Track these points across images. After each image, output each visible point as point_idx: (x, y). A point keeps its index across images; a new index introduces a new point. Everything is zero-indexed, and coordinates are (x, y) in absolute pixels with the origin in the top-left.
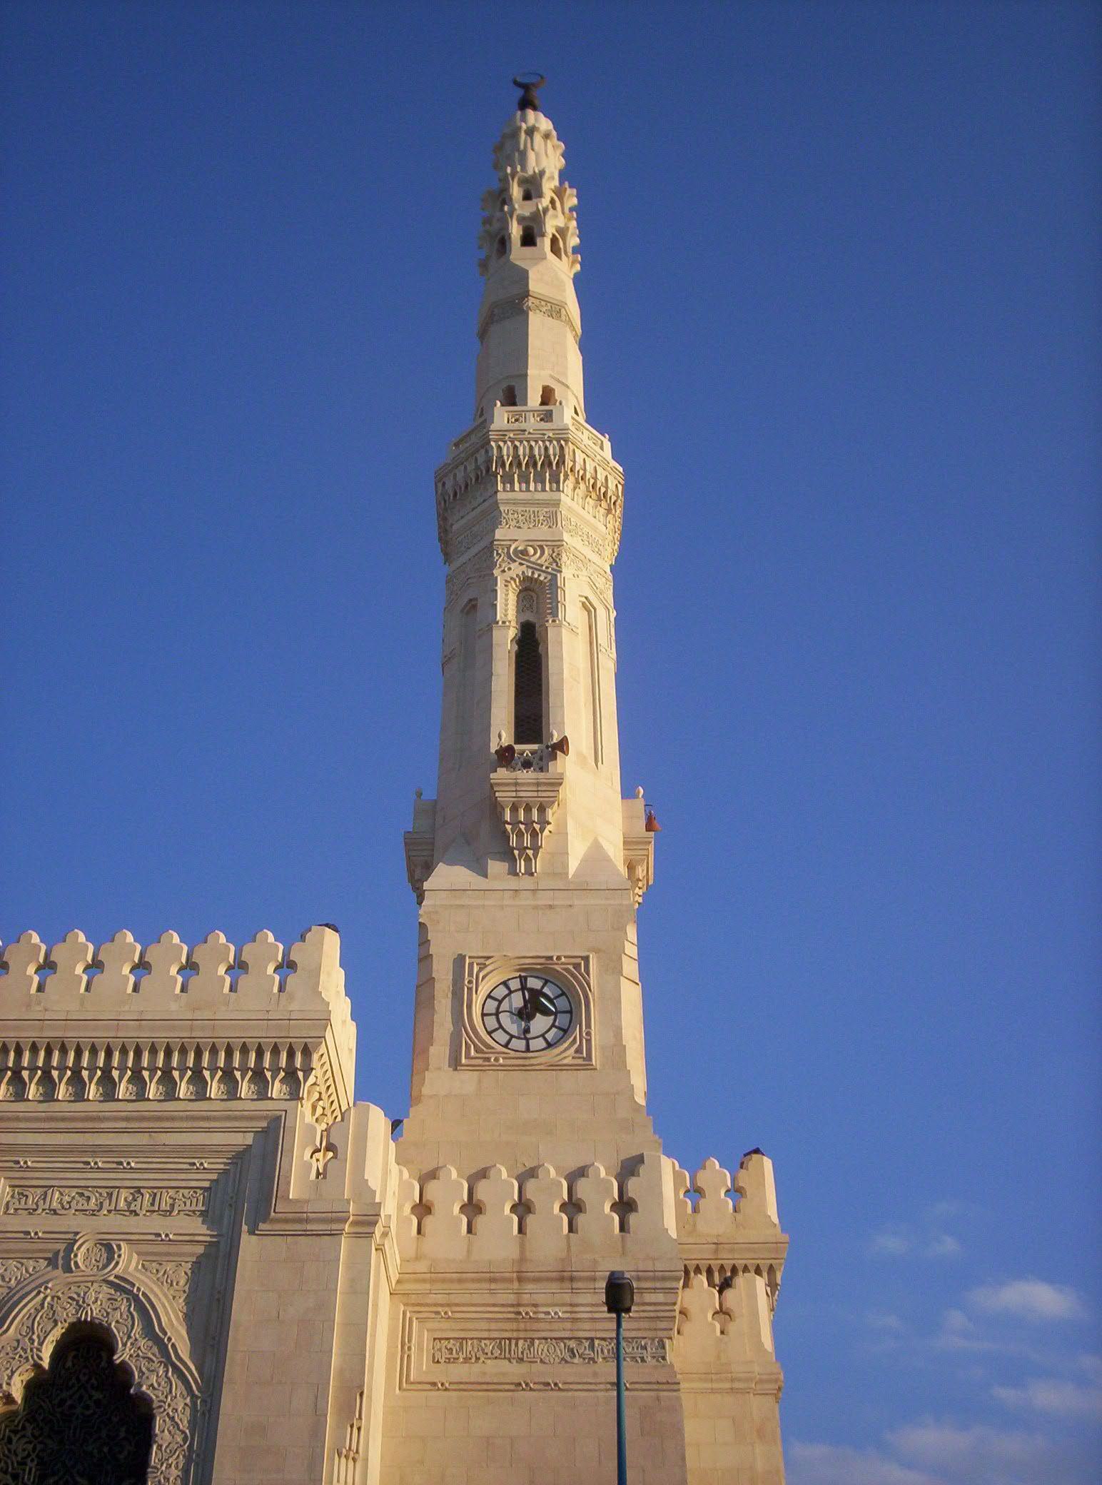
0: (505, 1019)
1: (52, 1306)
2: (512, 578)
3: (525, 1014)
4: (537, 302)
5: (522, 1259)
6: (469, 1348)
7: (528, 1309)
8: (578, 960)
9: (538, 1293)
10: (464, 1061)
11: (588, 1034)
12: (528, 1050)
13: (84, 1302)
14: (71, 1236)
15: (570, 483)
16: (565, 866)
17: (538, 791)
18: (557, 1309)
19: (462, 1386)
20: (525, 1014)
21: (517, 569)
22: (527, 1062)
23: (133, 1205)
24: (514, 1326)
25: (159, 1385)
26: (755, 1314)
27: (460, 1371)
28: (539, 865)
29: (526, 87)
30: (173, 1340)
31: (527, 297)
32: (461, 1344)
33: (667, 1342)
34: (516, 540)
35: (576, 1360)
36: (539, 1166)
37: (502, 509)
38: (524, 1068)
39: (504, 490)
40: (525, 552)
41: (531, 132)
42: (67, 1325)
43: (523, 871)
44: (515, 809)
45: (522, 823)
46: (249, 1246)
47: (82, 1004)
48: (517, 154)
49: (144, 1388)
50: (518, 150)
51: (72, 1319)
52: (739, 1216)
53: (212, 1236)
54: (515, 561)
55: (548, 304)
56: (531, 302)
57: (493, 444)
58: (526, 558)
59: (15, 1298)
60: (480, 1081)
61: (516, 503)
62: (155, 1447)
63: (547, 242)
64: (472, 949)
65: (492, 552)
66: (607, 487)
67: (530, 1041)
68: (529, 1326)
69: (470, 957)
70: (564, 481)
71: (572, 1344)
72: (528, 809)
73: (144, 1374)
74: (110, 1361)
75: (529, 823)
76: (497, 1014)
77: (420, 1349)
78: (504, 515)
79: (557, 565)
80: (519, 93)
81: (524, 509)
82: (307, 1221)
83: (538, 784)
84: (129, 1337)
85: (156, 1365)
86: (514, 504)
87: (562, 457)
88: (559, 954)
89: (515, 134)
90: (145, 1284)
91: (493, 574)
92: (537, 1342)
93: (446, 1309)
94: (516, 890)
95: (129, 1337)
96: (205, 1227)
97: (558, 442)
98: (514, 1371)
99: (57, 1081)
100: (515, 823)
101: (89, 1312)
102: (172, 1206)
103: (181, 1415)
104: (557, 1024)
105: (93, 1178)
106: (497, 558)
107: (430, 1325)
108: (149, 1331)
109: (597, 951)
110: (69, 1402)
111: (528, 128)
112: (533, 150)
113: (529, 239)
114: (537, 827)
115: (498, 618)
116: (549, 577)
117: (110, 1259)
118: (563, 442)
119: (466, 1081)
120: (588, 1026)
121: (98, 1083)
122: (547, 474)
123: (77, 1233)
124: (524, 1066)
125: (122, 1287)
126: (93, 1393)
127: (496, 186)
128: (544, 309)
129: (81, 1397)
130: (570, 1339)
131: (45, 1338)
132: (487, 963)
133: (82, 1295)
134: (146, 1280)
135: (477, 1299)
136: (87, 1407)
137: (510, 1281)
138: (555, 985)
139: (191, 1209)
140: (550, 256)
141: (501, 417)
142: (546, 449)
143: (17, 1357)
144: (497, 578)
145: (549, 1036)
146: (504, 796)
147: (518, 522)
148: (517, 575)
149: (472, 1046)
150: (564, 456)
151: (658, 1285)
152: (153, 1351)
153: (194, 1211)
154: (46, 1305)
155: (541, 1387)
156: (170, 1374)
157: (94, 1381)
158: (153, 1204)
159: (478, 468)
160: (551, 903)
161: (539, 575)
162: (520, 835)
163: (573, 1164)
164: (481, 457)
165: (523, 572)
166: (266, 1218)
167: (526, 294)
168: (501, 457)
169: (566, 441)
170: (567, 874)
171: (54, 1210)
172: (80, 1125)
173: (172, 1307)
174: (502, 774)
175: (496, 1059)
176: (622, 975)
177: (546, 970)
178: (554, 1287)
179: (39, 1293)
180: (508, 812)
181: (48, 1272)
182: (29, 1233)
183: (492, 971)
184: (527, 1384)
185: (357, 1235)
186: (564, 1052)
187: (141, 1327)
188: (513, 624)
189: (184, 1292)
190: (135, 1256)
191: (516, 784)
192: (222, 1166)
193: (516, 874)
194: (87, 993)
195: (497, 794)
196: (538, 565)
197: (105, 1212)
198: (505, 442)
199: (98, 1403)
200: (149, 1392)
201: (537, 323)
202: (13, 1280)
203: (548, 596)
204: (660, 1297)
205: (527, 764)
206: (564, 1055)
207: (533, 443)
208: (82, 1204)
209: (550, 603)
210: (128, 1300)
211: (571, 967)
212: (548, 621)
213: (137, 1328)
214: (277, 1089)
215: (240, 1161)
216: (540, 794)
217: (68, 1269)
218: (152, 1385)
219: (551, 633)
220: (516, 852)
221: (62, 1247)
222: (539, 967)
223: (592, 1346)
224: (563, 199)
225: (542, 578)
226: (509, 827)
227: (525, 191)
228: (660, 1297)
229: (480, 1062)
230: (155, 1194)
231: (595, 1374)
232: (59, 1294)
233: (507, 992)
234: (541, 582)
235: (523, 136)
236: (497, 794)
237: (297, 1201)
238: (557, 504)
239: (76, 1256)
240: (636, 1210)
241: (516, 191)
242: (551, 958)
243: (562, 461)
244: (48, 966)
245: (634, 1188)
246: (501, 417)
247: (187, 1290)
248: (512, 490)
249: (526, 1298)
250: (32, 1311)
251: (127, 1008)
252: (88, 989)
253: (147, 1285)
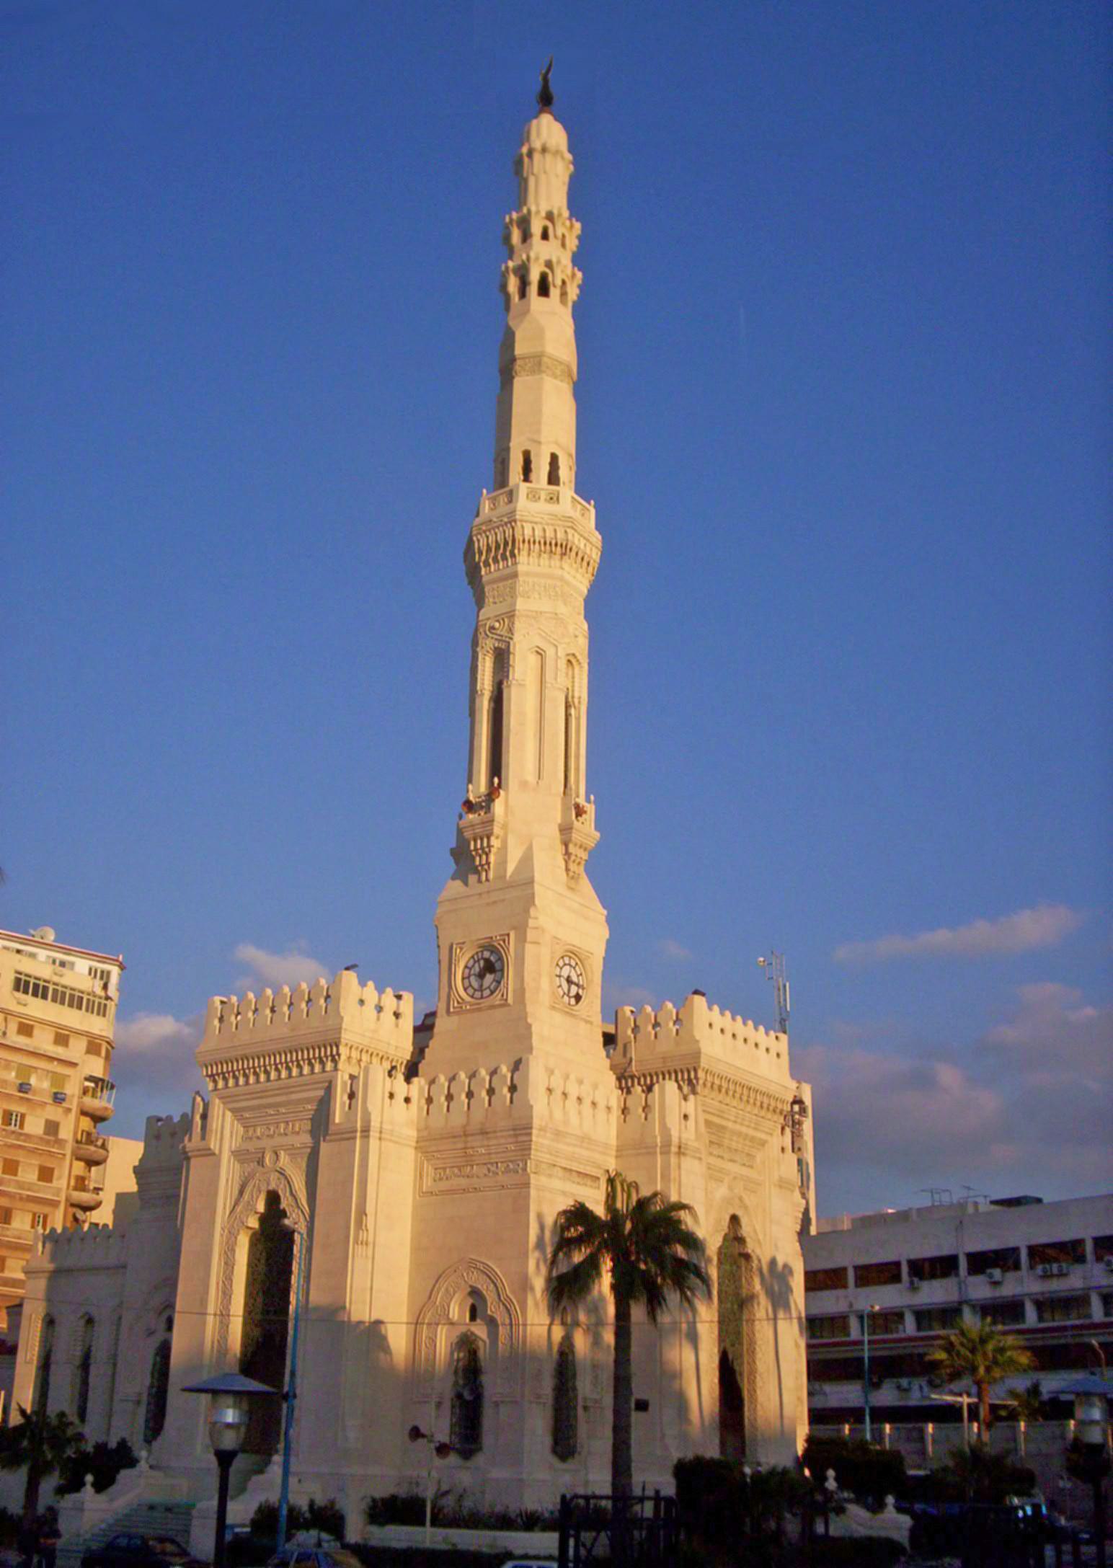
0: (472, 978)
3: (481, 976)
15: (524, 553)
16: (505, 871)
20: (481, 976)
24: (464, 1159)
35: (491, 1174)
52: (678, 1038)
74: (279, 1208)
98: (463, 1182)
107: (432, 1162)
109: (514, 928)
114: (487, 850)
137: (460, 1136)
170: (505, 876)
172: (259, 1095)
178: (480, 1137)
190: (229, 1114)
214: (329, 1066)
217: (263, 1166)
220: (480, 868)
237: (337, 1124)
249: (469, 1145)
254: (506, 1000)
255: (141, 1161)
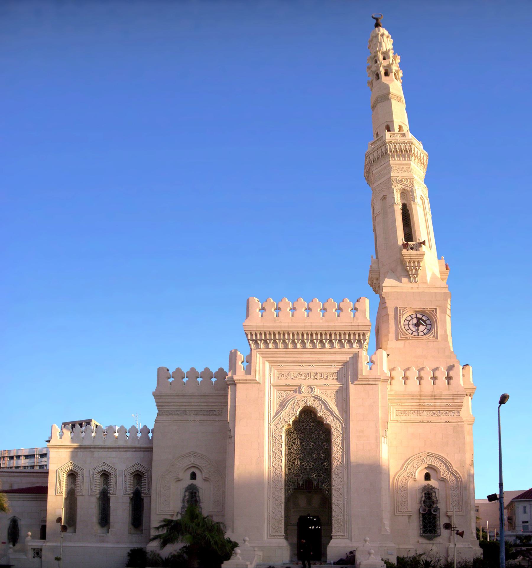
0: (411, 326)
1: (298, 403)
2: (398, 189)
3: (417, 325)
4: (393, 96)
5: (421, 391)
6: (406, 413)
7: (422, 403)
8: (433, 309)
9: (426, 400)
10: (399, 338)
11: (437, 331)
12: (418, 335)
13: (307, 401)
14: (299, 385)
16: (426, 280)
17: (417, 257)
18: (430, 403)
19: (405, 421)
20: (417, 325)
21: (400, 186)
22: (419, 339)
23: (315, 377)
24: (419, 407)
25: (332, 421)
26: (468, 406)
27: (404, 418)
28: (418, 279)
29: (377, 19)
30: (334, 411)
31: (390, 94)
32: (404, 411)
33: (460, 412)
34: (398, 177)
36: (425, 367)
37: (392, 166)
38: (418, 341)
39: (392, 160)
40: (401, 180)
41: (382, 35)
42: (302, 407)
43: (413, 281)
44: (410, 262)
45: (412, 267)
46: (352, 387)
47: (292, 320)
48: (378, 43)
49: (328, 422)
50: (379, 42)
51: (304, 406)
53: (340, 385)
54: (399, 183)
55: (397, 97)
56: (391, 96)
57: (387, 144)
58: (403, 182)
59: (287, 400)
60: (404, 344)
61: (396, 164)
62: (333, 435)
63: (393, 74)
64: (400, 305)
65: (391, 180)
66: (424, 160)
67: (419, 333)
68: (422, 407)
69: (399, 308)
70: (412, 157)
71: (434, 412)
72: (414, 262)
73: (327, 419)
75: (415, 267)
76: (408, 325)
77: (393, 413)
78: (393, 168)
79: (413, 185)
80: (375, 21)
81: (399, 166)
82: (369, 381)
83: (417, 255)
84: (321, 410)
85: (330, 417)
86: (396, 164)
87: (411, 149)
88: (427, 307)
89: (377, 36)
90: (323, 397)
91: (392, 188)
92: (425, 411)
93: (400, 403)
94: (412, 287)
95: (321, 410)
96: (338, 382)
97: (409, 144)
99: (288, 343)
100: (410, 267)
101: (309, 404)
102: (327, 377)
103: (339, 428)
104: (427, 328)
105: (302, 370)
106: (393, 182)
108: (326, 408)
109: (439, 307)
110: (305, 426)
111: (381, 34)
112: (384, 42)
113: (387, 74)
114: (417, 268)
115: (395, 202)
116: (411, 189)
117: (312, 391)
118: (411, 144)
119: (400, 344)
120: (437, 329)
121: (300, 344)
122: (406, 155)
123: (301, 384)
124: (418, 340)
125: (316, 397)
126: (311, 423)
127: (373, 55)
128: (395, 98)
129: (308, 425)
130: (434, 411)
131: (297, 410)
132: (405, 309)
133: (306, 400)
134: (324, 396)
135: (408, 401)
136: (310, 427)
138: (426, 316)
139: (333, 378)
140: (395, 80)
141: (388, 135)
142: (405, 146)
143: (290, 415)
144: (393, 189)
145: (425, 332)
146: (407, 258)
147: (398, 170)
148: (400, 188)
149: (402, 334)
150: (412, 149)
151: (459, 398)
152: (328, 413)
153: (334, 378)
154: (296, 402)
155: (427, 422)
156: (334, 419)
157: (311, 420)
158: (321, 376)
159: (382, 152)
160: (423, 291)
161: (407, 188)
162: (412, 270)
163: (434, 367)
164: (383, 149)
165: (402, 187)
166: (356, 380)
167: (389, 93)
168: (390, 149)
169: (412, 144)
170: (427, 282)
171: (292, 378)
173: (332, 402)
174: (404, 251)
175: (409, 338)
176: (447, 314)
177: (423, 313)
178: (430, 398)
179: (293, 399)
180: (407, 263)
181: (294, 394)
182: (287, 384)
183: (406, 312)
184: (423, 421)
185: (383, 385)
186: (430, 336)
187: (324, 407)
188: (401, 204)
189: (334, 399)
190: (319, 390)
191: (410, 255)
192: (340, 366)
193: (412, 282)
194: (292, 317)
195: (404, 258)
196: (407, 185)
197: (308, 379)
198: (391, 144)
199: (313, 426)
200: (329, 423)
201: (394, 103)
202: (284, 396)
203: (411, 195)
204: (459, 401)
205: (412, 248)
206: (429, 337)
207: (401, 144)
208: (300, 376)
209: (412, 197)
210: (319, 401)
211: (431, 311)
212: (412, 203)
213: (323, 408)
215: (345, 365)
216: (418, 258)
218: (330, 421)
219: (413, 207)
220: (411, 275)
221: (297, 388)
222: (421, 311)
223: (440, 412)
224: (396, 60)
225: (408, 189)
226: (408, 268)
227: (383, 57)
228: (459, 401)
229: (404, 338)
230: (321, 374)
231: (441, 419)
232: (299, 399)
233: (411, 318)
234: (408, 190)
235: (380, 36)
236: (404, 258)
238: (410, 165)
239: (302, 390)
240: (452, 379)
241: (381, 57)
242: (425, 308)
243: (410, 151)
244: (278, 309)
245: (452, 373)
246: (388, 135)
247: (335, 398)
248: (395, 160)
249: (422, 401)
250: (292, 404)
251: (306, 322)
252: (292, 316)
253: (324, 397)
254: (437, 338)
255: (156, 390)
